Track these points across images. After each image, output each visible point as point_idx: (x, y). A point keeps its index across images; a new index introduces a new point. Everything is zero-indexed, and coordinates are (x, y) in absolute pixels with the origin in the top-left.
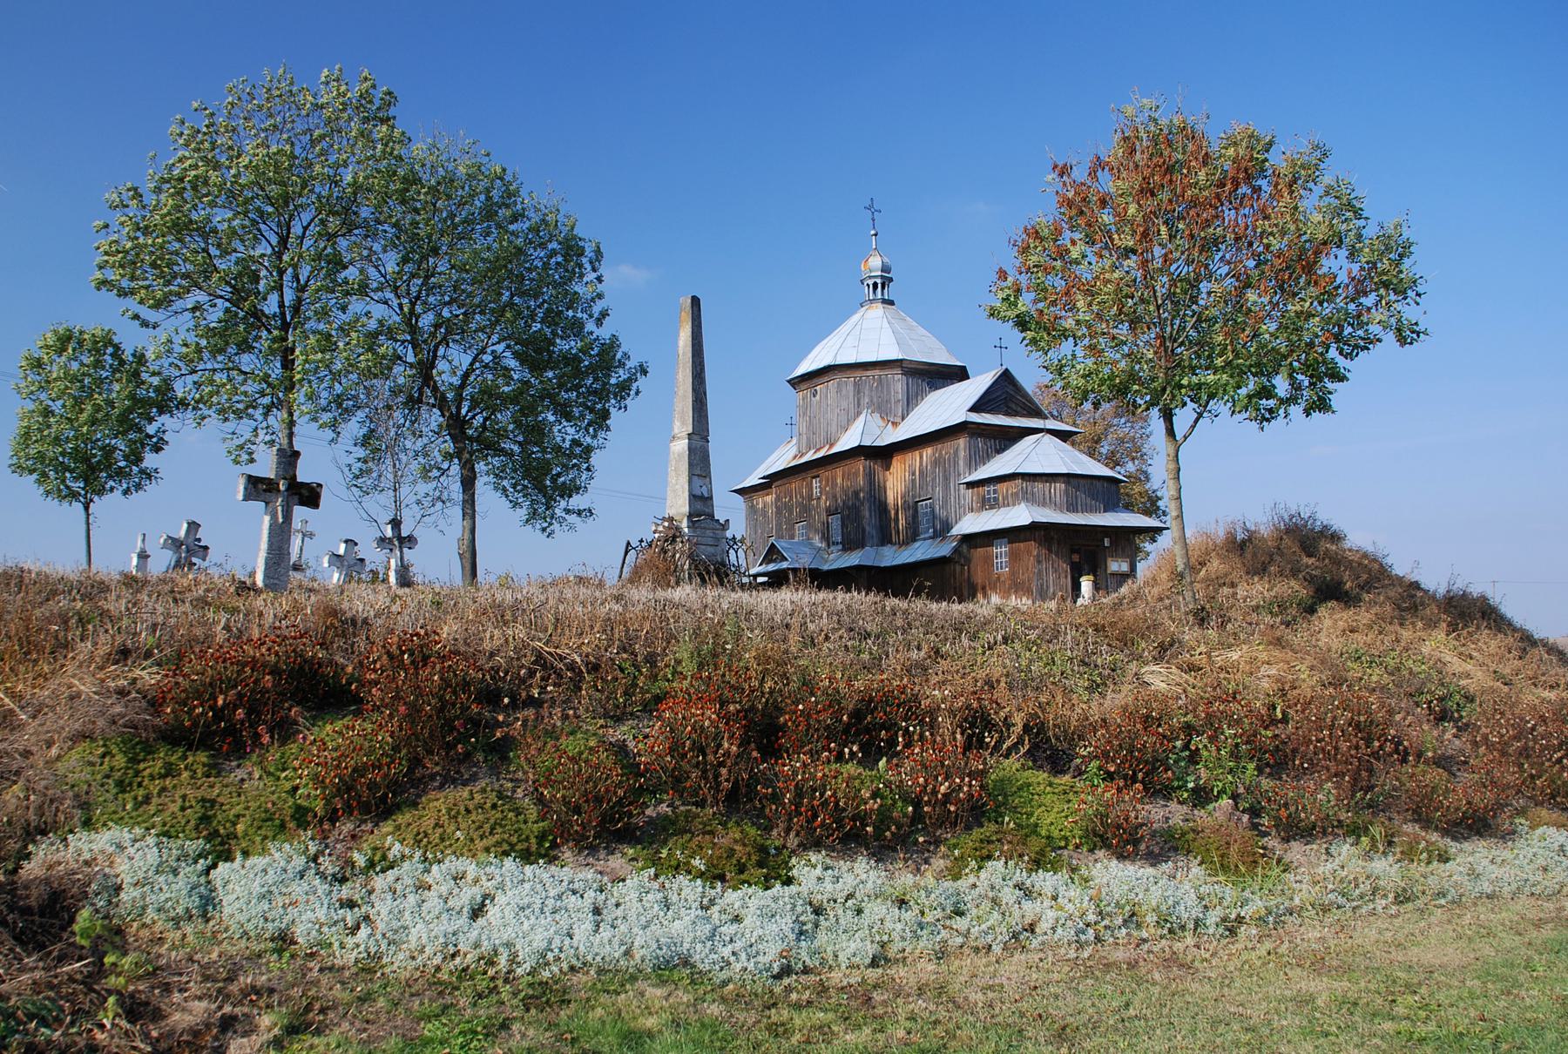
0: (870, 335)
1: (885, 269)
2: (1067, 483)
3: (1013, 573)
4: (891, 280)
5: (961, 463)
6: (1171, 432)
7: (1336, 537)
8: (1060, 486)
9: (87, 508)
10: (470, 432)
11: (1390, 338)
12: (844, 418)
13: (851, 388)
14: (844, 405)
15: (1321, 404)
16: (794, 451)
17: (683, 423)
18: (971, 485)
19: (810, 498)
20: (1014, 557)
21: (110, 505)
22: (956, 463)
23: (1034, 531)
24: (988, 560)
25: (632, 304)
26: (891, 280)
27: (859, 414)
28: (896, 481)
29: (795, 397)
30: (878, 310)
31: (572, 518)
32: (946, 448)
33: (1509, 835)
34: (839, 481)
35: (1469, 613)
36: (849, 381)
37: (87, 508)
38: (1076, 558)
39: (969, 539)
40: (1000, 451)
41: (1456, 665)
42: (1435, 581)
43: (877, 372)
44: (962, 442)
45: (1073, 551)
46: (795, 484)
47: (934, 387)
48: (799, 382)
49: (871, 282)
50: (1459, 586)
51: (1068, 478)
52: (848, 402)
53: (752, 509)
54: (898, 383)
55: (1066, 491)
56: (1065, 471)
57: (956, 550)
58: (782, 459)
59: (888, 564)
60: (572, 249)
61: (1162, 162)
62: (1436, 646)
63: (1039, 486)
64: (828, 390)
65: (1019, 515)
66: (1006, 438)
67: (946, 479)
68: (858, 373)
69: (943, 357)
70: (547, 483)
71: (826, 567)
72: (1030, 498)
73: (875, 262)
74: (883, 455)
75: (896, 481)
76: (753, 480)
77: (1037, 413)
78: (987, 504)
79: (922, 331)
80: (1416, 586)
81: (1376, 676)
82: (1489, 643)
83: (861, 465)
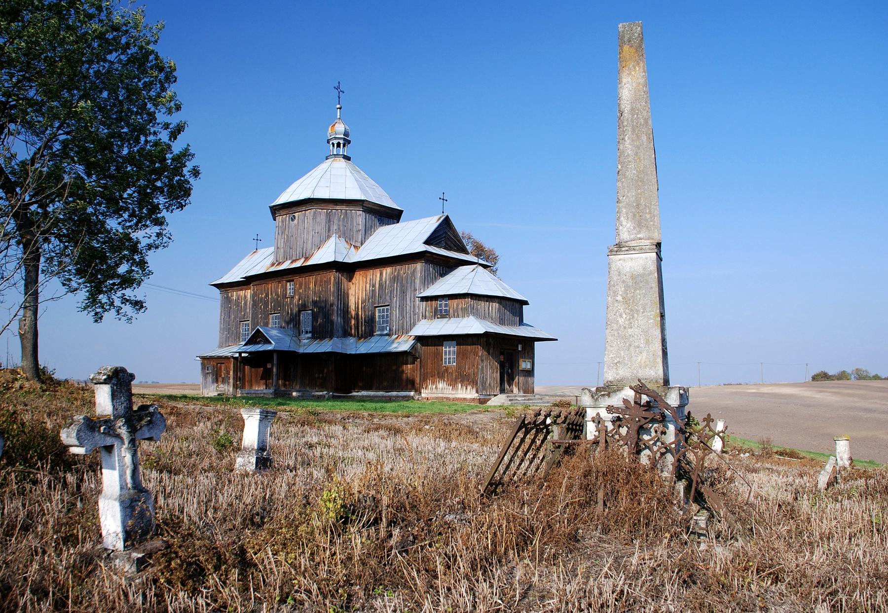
0: (335, 179)
2: (500, 303)
3: (459, 366)
4: (349, 142)
5: (418, 281)
8: (495, 305)
12: (317, 242)
13: (323, 217)
14: (318, 228)
16: (271, 259)
18: (425, 299)
19: (285, 296)
23: (487, 340)
24: (438, 356)
25: (202, 120)
26: (349, 142)
27: (329, 237)
30: (341, 163)
31: (127, 309)
32: (404, 270)
34: (312, 286)
36: (322, 213)
39: (421, 340)
40: (442, 275)
43: (344, 208)
44: (419, 266)
45: (502, 353)
46: (272, 286)
47: (382, 223)
48: (276, 210)
49: (335, 142)
52: (321, 227)
53: (227, 300)
54: (359, 217)
55: (499, 309)
57: (413, 347)
58: (260, 262)
59: (353, 352)
60: (143, 60)
63: (482, 304)
64: (307, 217)
65: (472, 325)
66: (447, 266)
67: (403, 292)
68: (331, 207)
69: (387, 202)
70: (107, 271)
73: (340, 128)
74: (349, 269)
75: (358, 290)
76: (235, 275)
77: (464, 250)
78: (440, 314)
83: (333, 276)
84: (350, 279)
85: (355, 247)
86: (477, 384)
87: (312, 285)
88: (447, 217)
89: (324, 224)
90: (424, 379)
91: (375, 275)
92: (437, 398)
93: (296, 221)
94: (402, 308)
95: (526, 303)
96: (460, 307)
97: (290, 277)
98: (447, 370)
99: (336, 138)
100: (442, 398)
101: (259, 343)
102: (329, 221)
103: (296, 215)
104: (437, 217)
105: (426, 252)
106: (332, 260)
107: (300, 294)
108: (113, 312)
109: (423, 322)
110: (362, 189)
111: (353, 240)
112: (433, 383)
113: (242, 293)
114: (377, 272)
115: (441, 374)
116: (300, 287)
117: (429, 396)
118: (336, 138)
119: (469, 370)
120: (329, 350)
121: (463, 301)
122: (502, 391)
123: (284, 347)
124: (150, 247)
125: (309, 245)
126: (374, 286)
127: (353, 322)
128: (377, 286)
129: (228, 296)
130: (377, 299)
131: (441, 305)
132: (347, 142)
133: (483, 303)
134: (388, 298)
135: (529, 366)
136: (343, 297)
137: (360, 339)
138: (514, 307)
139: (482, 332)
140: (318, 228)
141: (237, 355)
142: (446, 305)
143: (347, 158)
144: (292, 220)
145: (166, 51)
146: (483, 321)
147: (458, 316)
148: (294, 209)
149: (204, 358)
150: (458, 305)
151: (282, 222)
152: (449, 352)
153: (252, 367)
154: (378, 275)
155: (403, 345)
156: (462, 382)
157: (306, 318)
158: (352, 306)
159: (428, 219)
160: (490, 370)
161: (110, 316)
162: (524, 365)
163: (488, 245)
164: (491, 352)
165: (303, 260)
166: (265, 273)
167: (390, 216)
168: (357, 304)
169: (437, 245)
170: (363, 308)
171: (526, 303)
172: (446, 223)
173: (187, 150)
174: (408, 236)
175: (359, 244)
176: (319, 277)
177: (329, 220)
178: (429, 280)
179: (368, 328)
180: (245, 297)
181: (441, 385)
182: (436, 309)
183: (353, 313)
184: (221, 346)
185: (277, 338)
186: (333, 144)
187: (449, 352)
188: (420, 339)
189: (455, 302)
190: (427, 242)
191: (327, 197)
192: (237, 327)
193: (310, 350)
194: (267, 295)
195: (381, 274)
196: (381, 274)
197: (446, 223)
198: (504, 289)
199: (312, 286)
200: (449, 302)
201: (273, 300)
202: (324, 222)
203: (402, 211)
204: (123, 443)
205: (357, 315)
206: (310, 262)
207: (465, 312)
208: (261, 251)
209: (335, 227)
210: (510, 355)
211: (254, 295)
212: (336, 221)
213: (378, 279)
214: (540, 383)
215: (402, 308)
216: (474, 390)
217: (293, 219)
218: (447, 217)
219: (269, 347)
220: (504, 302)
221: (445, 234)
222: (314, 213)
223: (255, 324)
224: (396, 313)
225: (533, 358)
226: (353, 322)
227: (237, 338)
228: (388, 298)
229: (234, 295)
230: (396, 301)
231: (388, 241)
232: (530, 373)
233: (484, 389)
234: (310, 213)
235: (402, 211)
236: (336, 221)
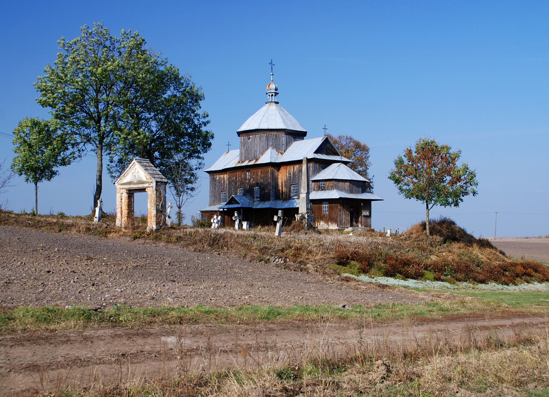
0: (269, 117)
1: (276, 89)
3: (330, 214)
6: (427, 207)
7: (454, 223)
8: (348, 184)
9: (36, 185)
11: (471, 194)
13: (264, 138)
14: (262, 144)
15: (456, 205)
16: (238, 159)
17: (304, 190)
18: (313, 181)
19: (246, 179)
20: (330, 209)
21: (44, 184)
23: (341, 201)
24: (320, 209)
27: (268, 149)
28: (282, 176)
29: (239, 139)
30: (273, 107)
31: (189, 192)
33: (487, 284)
34: (259, 174)
35: (484, 244)
36: (264, 135)
37: (36, 185)
38: (352, 210)
40: (324, 168)
41: (480, 256)
42: (477, 236)
43: (275, 133)
45: (351, 207)
46: (238, 173)
48: (240, 134)
49: (271, 94)
50: (482, 238)
51: (351, 181)
52: (263, 144)
53: (213, 180)
54: (283, 138)
56: (350, 179)
61: (429, 151)
62: (476, 251)
63: (341, 184)
64: (255, 139)
65: (334, 194)
66: (326, 164)
68: (268, 133)
71: (254, 207)
72: (338, 189)
73: (273, 86)
74: (277, 166)
75: (282, 176)
77: (336, 154)
79: (290, 116)
80: (472, 237)
81: (466, 258)
82: (488, 250)
83: (270, 169)
84: (278, 170)
85: (282, 153)
93: (250, 140)
97: (248, 169)
98: (324, 216)
101: (233, 204)
103: (251, 136)
104: (322, 138)
106: (269, 161)
107: (253, 178)
109: (314, 192)
110: (284, 122)
113: (222, 176)
114: (292, 167)
116: (254, 175)
119: (333, 216)
120: (268, 207)
121: (331, 182)
122: (352, 226)
123: (246, 206)
124: (196, 169)
125: (258, 153)
126: (290, 174)
129: (214, 178)
131: (322, 185)
132: (276, 94)
135: (367, 214)
136: (275, 179)
139: (338, 197)
140: (262, 144)
141: (222, 210)
143: (277, 103)
146: (339, 192)
149: (202, 212)
152: (325, 207)
153: (229, 216)
156: (331, 221)
158: (280, 184)
160: (345, 216)
163: (363, 142)
164: (345, 206)
165: (254, 161)
166: (235, 167)
167: (300, 135)
168: (282, 183)
170: (285, 185)
174: (303, 150)
175: (283, 152)
176: (263, 170)
180: (224, 178)
184: (210, 205)
185: (244, 202)
187: (325, 207)
189: (328, 183)
190: (316, 152)
191: (266, 128)
192: (220, 195)
193: (259, 207)
194: (236, 178)
195: (294, 168)
196: (294, 168)
197: (326, 142)
198: (353, 175)
199: (259, 174)
201: (239, 181)
202: (265, 141)
203: (306, 132)
206: (258, 162)
207: (332, 188)
208: (231, 152)
209: (271, 143)
211: (229, 178)
212: (271, 140)
219: (239, 206)
221: (327, 147)
223: (230, 194)
227: (220, 201)
229: (217, 177)
233: (341, 224)
234: (258, 136)
235: (306, 132)
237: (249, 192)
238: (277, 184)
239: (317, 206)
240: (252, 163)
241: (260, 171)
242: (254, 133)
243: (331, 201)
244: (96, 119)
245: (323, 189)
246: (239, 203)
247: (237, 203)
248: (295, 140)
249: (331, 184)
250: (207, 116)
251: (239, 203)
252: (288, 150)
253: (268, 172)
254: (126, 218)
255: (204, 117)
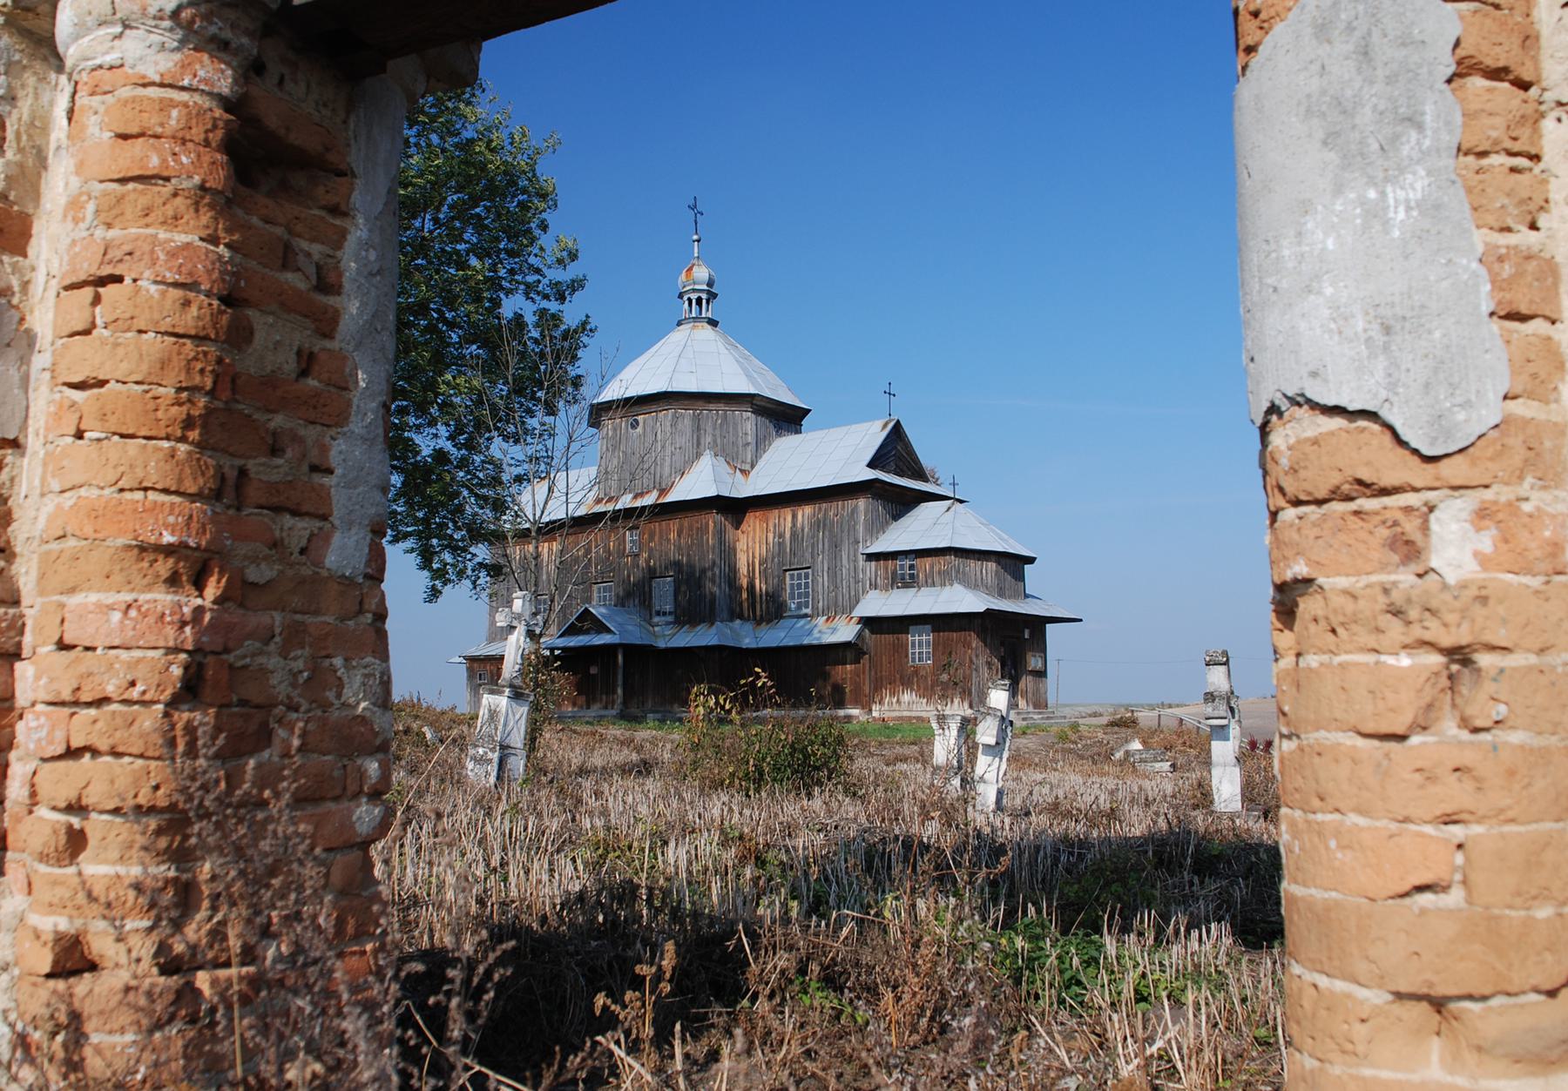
1: (710, 283)
2: (998, 563)
4: (715, 296)
8: (991, 566)
10: (412, 1043)
13: (687, 422)
18: (871, 557)
19: (622, 554)
20: (943, 653)
22: (853, 528)
24: (901, 650)
26: (715, 296)
27: (698, 456)
30: (706, 332)
39: (872, 624)
40: (896, 517)
43: (722, 406)
44: (862, 503)
45: (1002, 644)
49: (694, 296)
54: (748, 422)
57: (859, 635)
63: (973, 565)
66: (901, 503)
67: (836, 546)
71: (661, 644)
72: (973, 585)
73: (702, 273)
74: (734, 509)
75: (752, 544)
83: (713, 520)
86: (970, 694)
87: (672, 539)
88: (898, 425)
89: (689, 434)
90: (877, 687)
91: (785, 519)
92: (901, 718)
93: (640, 430)
94: (833, 573)
95: (1031, 560)
96: (936, 569)
99: (694, 291)
100: (910, 718)
101: (587, 632)
102: (699, 429)
103: (640, 418)
104: (880, 423)
105: (876, 480)
107: (651, 550)
108: (467, 583)
109: (873, 594)
111: (740, 460)
112: (893, 694)
114: (787, 513)
115: (906, 679)
116: (651, 538)
117: (887, 715)
118: (694, 291)
120: (714, 642)
121: (942, 559)
125: (667, 470)
126: (781, 536)
127: (745, 595)
128: (788, 535)
130: (787, 560)
131: (904, 567)
132: (712, 296)
133: (972, 563)
134: (808, 555)
135: (1039, 665)
137: (759, 624)
138: (1013, 565)
142: (912, 567)
143: (713, 323)
144: (633, 427)
145: (547, 172)
147: (933, 585)
148: (636, 409)
149: (472, 660)
150: (932, 567)
151: (615, 430)
152: (920, 644)
154: (789, 518)
155: (844, 631)
157: (664, 591)
159: (866, 425)
161: (457, 594)
162: (1034, 662)
165: (655, 494)
167: (787, 418)
168: (751, 566)
169: (883, 469)
170: (764, 573)
171: (1031, 560)
172: (897, 434)
173: (584, 324)
175: (747, 467)
177: (698, 429)
178: (876, 528)
179: (773, 609)
181: (907, 697)
182: (894, 573)
183: (744, 582)
185: (622, 629)
186: (690, 300)
187: (920, 644)
188: (869, 623)
195: (794, 517)
196: (794, 517)
197: (897, 434)
200: (917, 562)
204: (201, 239)
205: (751, 586)
206: (670, 498)
207: (946, 579)
209: (709, 439)
210: (1014, 642)
212: (709, 430)
213: (789, 525)
214: (1053, 686)
215: (833, 573)
216: (966, 705)
217: (635, 425)
218: (898, 425)
220: (1003, 561)
221: (895, 450)
222: (674, 415)
224: (824, 580)
225: (1044, 651)
226: (745, 595)
228: (808, 555)
230: (822, 562)
231: (790, 464)
232: (1041, 674)
236: (709, 430)
237: (637, 595)
238: (733, 570)
239: (890, 638)
240: (649, 500)
241: (674, 525)
242: (654, 408)
243: (940, 623)
244: (259, 866)
245: (909, 582)
246: (609, 631)
247: (602, 628)
248: (779, 435)
249: (941, 563)
250: (573, 256)
251: (609, 631)
252: (761, 463)
253: (703, 530)
254: (116, 861)
255: (560, 261)
